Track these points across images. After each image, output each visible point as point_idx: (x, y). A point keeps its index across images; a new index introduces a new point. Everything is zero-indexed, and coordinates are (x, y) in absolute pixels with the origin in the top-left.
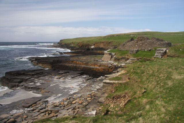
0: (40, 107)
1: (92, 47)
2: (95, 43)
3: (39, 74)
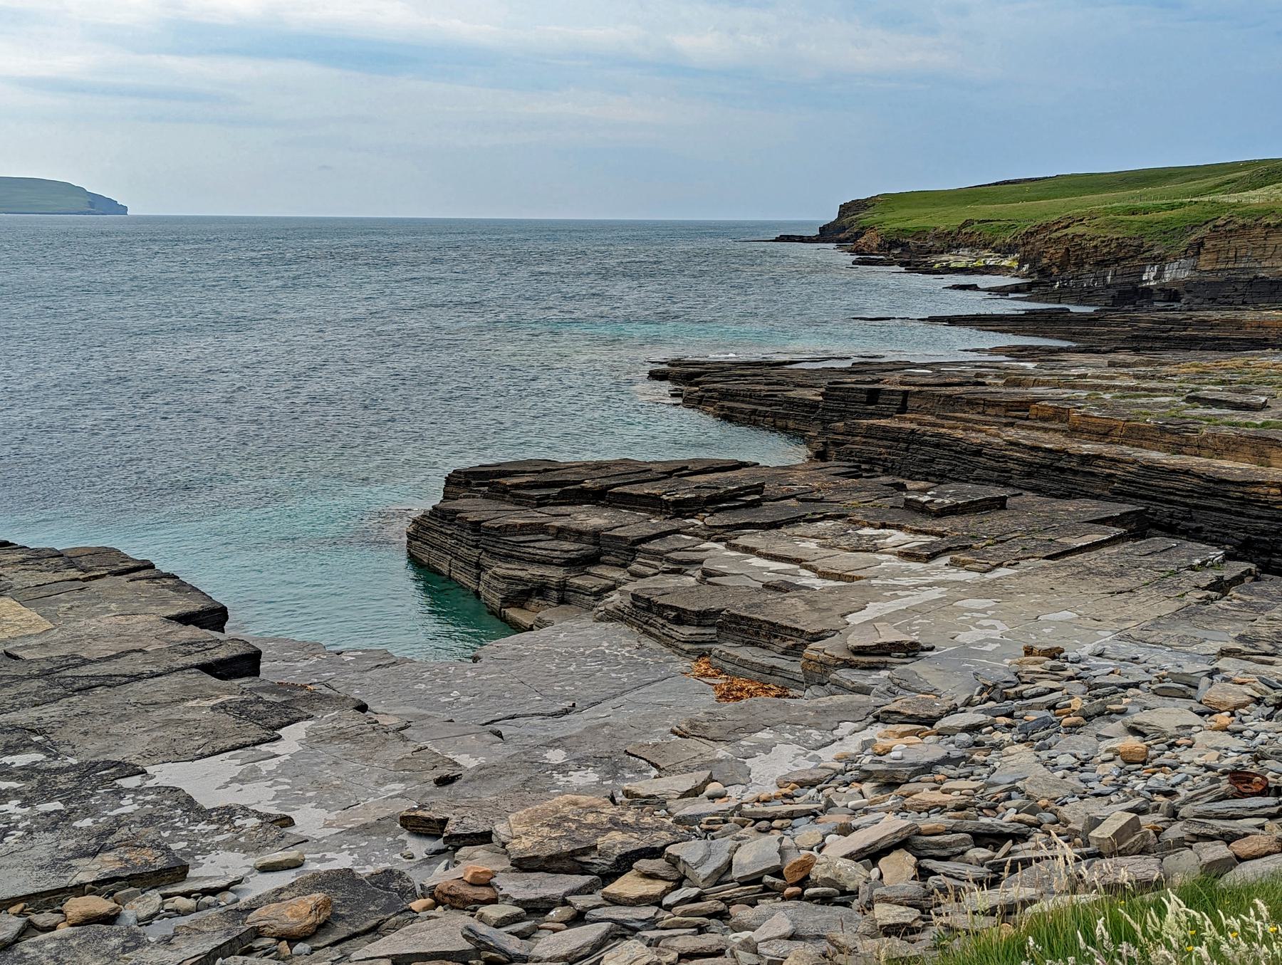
0: (358, 332)
1: (1175, 273)
2: (1204, 232)
3: (736, 503)
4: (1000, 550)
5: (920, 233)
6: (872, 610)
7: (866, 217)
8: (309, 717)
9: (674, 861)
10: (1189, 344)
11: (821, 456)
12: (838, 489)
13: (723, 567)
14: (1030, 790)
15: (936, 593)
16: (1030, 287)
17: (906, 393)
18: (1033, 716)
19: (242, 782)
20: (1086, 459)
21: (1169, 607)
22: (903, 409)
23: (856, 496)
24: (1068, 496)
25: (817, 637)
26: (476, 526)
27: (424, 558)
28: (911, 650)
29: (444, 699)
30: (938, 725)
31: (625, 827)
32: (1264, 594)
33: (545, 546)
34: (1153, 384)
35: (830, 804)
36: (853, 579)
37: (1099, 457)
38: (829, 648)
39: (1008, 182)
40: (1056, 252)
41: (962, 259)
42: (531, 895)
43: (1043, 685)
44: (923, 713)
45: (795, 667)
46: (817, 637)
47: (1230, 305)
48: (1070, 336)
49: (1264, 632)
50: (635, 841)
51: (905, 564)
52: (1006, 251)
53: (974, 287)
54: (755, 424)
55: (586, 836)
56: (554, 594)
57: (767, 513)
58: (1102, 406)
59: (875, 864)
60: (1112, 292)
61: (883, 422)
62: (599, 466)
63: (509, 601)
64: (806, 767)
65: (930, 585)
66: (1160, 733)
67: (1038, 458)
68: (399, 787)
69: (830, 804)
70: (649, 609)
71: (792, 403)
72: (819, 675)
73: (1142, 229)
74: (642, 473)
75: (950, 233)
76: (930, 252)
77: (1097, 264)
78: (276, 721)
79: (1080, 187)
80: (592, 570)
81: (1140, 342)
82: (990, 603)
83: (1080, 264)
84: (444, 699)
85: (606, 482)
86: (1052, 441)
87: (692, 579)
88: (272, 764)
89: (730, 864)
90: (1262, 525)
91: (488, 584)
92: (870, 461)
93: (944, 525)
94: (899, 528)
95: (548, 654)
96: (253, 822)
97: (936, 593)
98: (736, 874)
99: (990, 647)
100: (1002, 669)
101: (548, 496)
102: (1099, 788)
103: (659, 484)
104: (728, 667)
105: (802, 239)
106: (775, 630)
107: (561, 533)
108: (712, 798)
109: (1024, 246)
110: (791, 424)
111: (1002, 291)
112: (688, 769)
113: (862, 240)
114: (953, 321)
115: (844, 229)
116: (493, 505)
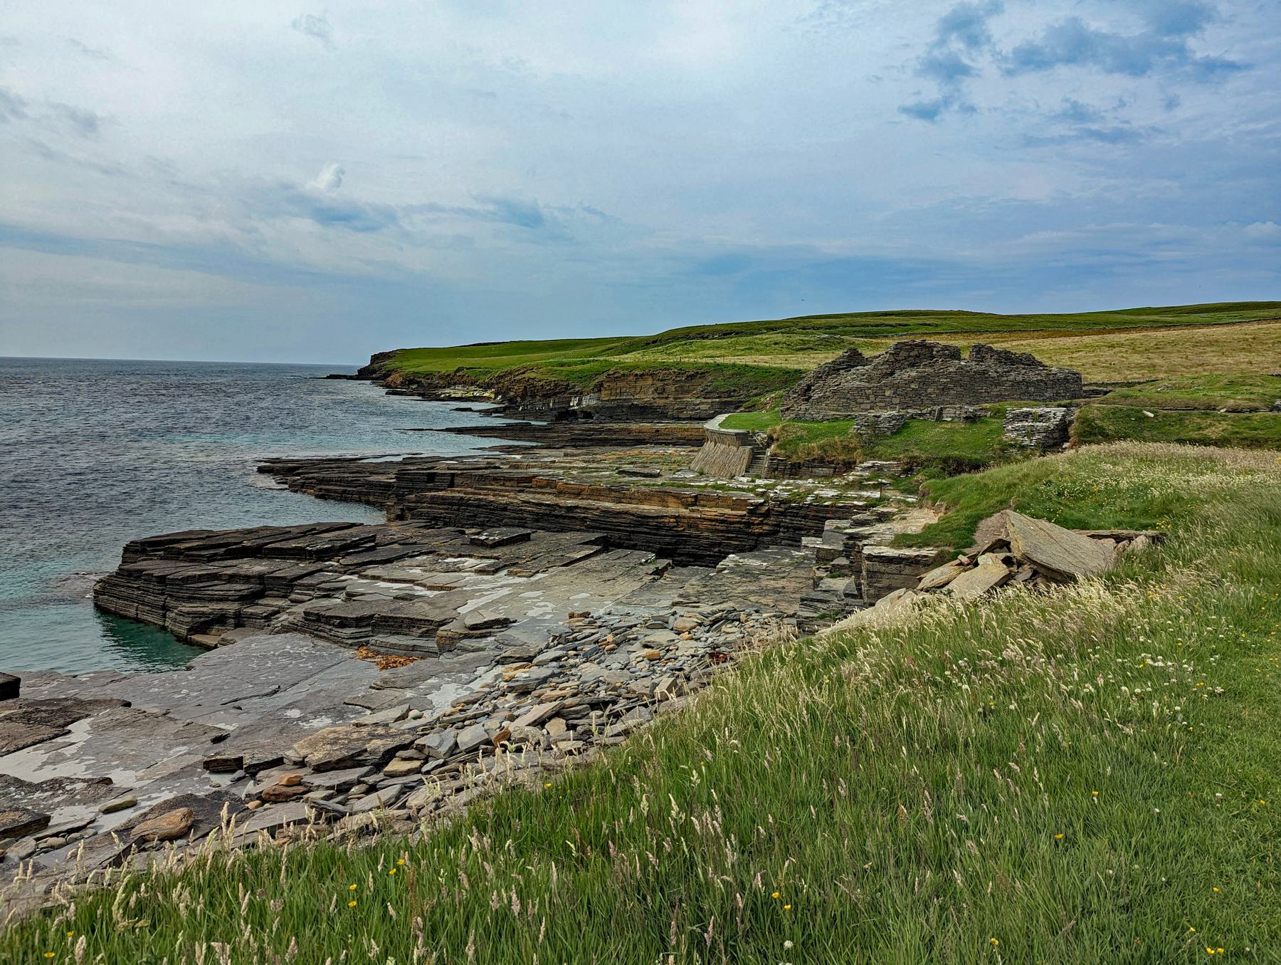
1: (589, 401)
3: (359, 550)
4: (536, 563)
5: (428, 375)
6: (472, 605)
7: (390, 365)
8: (87, 716)
9: (421, 748)
10: (604, 442)
11: (400, 517)
12: (424, 536)
13: (361, 590)
14: (608, 680)
15: (506, 591)
16: (505, 409)
17: (453, 475)
18: (587, 648)
19: (54, 763)
20: (570, 509)
21: (637, 585)
22: (452, 485)
23: (437, 538)
24: (562, 530)
25: (443, 623)
26: (162, 580)
27: (112, 607)
28: (505, 623)
29: (177, 696)
30: (535, 661)
31: (380, 737)
32: (682, 574)
33: (220, 588)
34: (595, 465)
35: (495, 708)
36: (451, 588)
37: (577, 507)
38: (453, 628)
40: (519, 388)
41: (458, 392)
42: (336, 782)
43: (587, 632)
44: (525, 655)
45: (432, 644)
46: (443, 623)
47: (620, 420)
48: (536, 439)
49: (691, 592)
50: (390, 743)
51: (480, 577)
52: (487, 387)
53: (470, 410)
54: (345, 500)
55: (358, 746)
56: (232, 621)
57: (381, 554)
58: (574, 478)
59: (543, 727)
60: (555, 412)
61: (441, 493)
62: (250, 532)
63: (195, 630)
64: (464, 694)
65: (502, 587)
66: (659, 646)
67: (542, 510)
68: (184, 749)
69: (495, 708)
70: (318, 620)
71: (371, 484)
72: (449, 645)
74: (285, 534)
78: (61, 721)
80: (260, 602)
81: (578, 442)
82: (540, 593)
83: (533, 396)
84: (177, 696)
85: (260, 541)
86: (549, 499)
87: (339, 601)
88: (73, 749)
89: (456, 744)
90: (667, 539)
91: (174, 620)
92: (435, 518)
93: (498, 552)
94: (470, 556)
95: (248, 658)
96: (79, 786)
97: (506, 591)
98: (462, 748)
99: (548, 617)
100: (562, 625)
101: (216, 554)
102: (643, 674)
103: (301, 540)
104: (382, 650)
106: (413, 623)
107: (232, 578)
108: (415, 718)
109: (499, 384)
110: (371, 498)
111: (487, 413)
112: (391, 706)
113: (390, 379)
114: (460, 431)
115: (374, 372)
116: (171, 564)
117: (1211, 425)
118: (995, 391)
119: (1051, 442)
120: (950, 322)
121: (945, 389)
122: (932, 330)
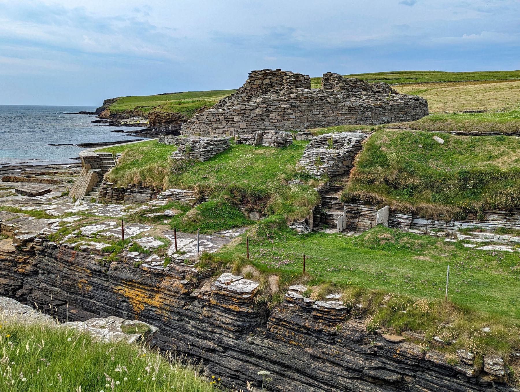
39: (167, 94)
73: (180, 110)
75: (131, 111)
76: (124, 118)
77: (166, 122)
79: (188, 96)
83: (160, 123)
105: (89, 113)
117: (503, 154)
118: (332, 116)
119: (341, 170)
120: (425, 77)
121: (285, 114)
122: (413, 81)
